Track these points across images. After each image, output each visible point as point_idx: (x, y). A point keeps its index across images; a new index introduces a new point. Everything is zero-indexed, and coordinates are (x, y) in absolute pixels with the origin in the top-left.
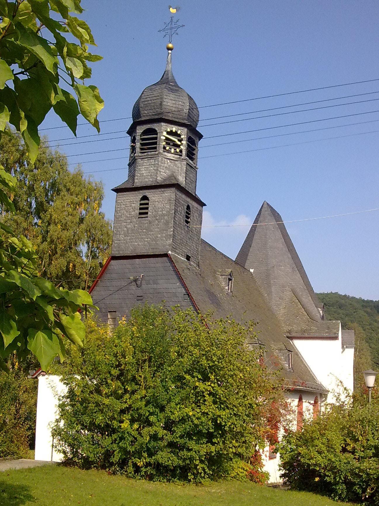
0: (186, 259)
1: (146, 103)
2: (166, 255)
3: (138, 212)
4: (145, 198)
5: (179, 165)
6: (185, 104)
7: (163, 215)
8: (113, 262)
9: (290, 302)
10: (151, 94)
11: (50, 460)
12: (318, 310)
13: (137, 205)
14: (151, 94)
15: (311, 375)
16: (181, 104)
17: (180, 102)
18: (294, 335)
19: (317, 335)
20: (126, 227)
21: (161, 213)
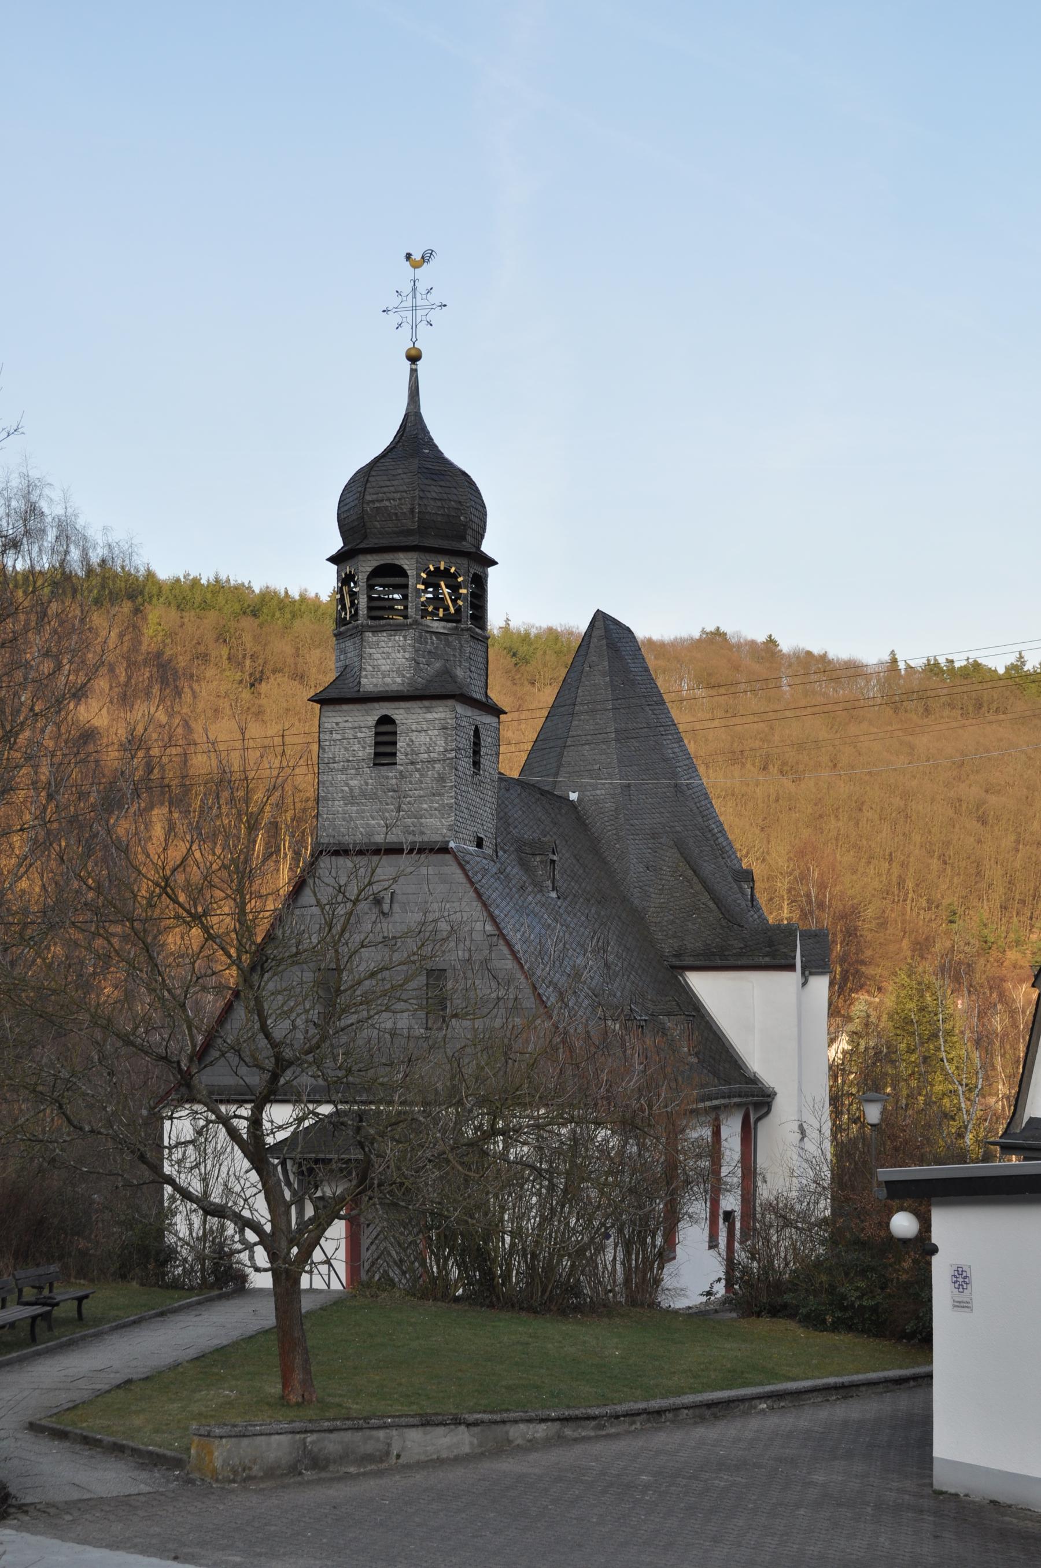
0: (477, 847)
1: (377, 505)
2: (444, 850)
3: (371, 750)
4: (386, 720)
5: (456, 643)
6: (462, 505)
7: (431, 761)
8: (325, 862)
9: (672, 876)
10: (388, 483)
11: (308, 1287)
12: (740, 888)
13: (368, 735)
14: (388, 483)
15: (732, 1057)
16: (455, 506)
17: (453, 503)
18: (688, 961)
19: (744, 961)
20: (347, 785)
21: (426, 756)
